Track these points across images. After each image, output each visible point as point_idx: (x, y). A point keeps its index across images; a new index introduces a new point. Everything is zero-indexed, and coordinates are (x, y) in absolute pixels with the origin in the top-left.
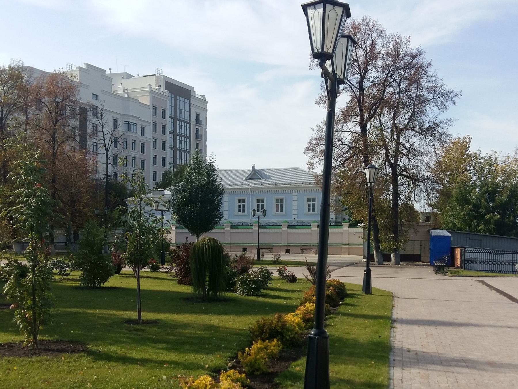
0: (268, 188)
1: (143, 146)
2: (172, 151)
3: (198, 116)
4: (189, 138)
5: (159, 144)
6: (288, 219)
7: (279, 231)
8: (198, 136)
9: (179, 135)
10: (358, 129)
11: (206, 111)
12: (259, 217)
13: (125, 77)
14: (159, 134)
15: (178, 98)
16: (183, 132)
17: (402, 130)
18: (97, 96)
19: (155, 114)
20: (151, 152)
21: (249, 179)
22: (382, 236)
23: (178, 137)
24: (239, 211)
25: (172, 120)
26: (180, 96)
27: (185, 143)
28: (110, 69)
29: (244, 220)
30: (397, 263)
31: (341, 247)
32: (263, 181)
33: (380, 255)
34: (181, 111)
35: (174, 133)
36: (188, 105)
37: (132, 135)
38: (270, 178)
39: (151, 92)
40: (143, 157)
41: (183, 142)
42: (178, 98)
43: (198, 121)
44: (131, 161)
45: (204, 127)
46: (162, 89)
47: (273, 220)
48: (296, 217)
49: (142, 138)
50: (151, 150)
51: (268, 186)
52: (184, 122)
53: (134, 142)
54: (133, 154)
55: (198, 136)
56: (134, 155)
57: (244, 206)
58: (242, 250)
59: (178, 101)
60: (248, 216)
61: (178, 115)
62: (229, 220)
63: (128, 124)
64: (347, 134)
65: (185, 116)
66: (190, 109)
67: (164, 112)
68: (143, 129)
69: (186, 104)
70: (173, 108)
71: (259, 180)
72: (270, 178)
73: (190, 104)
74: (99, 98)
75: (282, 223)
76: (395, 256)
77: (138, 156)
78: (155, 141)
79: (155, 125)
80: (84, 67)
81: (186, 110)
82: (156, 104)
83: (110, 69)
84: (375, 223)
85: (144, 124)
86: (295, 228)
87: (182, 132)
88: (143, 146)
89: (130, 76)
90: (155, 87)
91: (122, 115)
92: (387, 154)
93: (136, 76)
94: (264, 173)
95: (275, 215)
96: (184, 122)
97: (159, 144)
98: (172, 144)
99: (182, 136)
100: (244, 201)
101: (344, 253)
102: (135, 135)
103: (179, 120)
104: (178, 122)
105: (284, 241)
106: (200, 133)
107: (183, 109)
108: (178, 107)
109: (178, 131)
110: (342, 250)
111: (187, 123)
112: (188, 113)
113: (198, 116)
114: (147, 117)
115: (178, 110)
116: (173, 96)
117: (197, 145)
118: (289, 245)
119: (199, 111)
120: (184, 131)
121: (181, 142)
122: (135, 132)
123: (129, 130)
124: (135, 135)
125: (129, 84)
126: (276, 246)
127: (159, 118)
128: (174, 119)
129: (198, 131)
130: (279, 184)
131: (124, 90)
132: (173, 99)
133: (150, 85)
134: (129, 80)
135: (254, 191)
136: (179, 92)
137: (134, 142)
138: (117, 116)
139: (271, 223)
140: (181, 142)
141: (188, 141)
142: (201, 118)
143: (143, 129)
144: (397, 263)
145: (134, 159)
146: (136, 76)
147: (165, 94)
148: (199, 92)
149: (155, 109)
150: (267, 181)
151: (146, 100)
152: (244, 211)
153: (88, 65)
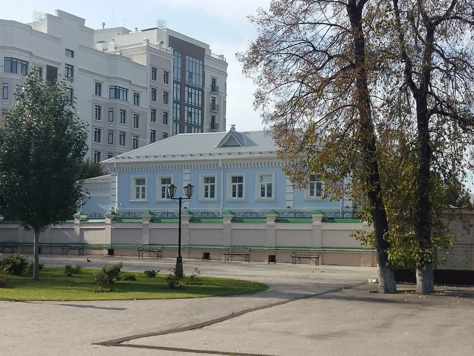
0: (248, 159)
1: (137, 118)
2: (178, 126)
3: (214, 81)
4: (202, 109)
5: (160, 116)
6: (277, 208)
7: (262, 226)
8: (213, 106)
9: (188, 106)
10: (344, 17)
11: (226, 75)
12: (180, 199)
13: (121, 33)
14: (159, 104)
15: (187, 57)
16: (193, 102)
17: (439, 19)
18: (72, 52)
19: (154, 77)
20: (148, 127)
21: (224, 146)
22: (393, 232)
23: (186, 108)
24: (206, 196)
25: (179, 86)
26: (189, 56)
27: (197, 115)
28: (104, 24)
29: (212, 208)
30: (428, 291)
31: (360, 254)
32: (242, 149)
33: (388, 273)
34: (191, 74)
35: (180, 103)
36: (201, 67)
37: (120, 103)
38: (255, 145)
39: (149, 48)
40: (136, 132)
41: (193, 114)
42: (187, 57)
43: (214, 88)
44: (118, 137)
45: (222, 96)
46: (165, 46)
47: (257, 209)
48: (291, 204)
49: (136, 108)
50: (148, 124)
51: (249, 156)
52: (196, 88)
53: (123, 113)
54: (119, 127)
55: (213, 106)
56: (124, 130)
57: (213, 187)
58: (202, 255)
59: (187, 62)
60: (218, 202)
61: (187, 80)
62: (188, 209)
63: (115, 89)
64: (322, 30)
65: (196, 81)
66: (204, 72)
67: (166, 75)
68: (137, 96)
69: (198, 65)
70: (179, 70)
71: (237, 148)
72: (255, 145)
73: (203, 66)
74: (75, 54)
75: (267, 213)
76: (424, 276)
77: (128, 131)
78: (154, 112)
79: (154, 91)
80: (55, 14)
81: (197, 73)
82: (156, 65)
83: (104, 24)
84: (377, 208)
85: (137, 90)
86: (287, 222)
87: (192, 100)
88: (137, 118)
89: (126, 32)
90: (155, 42)
91: (108, 77)
92: (408, 72)
93: (133, 30)
94: (247, 138)
95: (258, 202)
96: (196, 88)
97: (160, 116)
98: (178, 117)
99: (191, 106)
100: (213, 180)
101: (365, 264)
102: (128, 103)
103: (189, 86)
104: (186, 88)
105: (269, 242)
106: (216, 103)
107: (194, 71)
108: (187, 69)
109: (186, 99)
110: (362, 259)
111: (199, 90)
112: (201, 77)
113: (214, 81)
114: (143, 81)
115: (187, 74)
116: (180, 55)
117: (213, 118)
118: (277, 249)
119: (215, 75)
120: (195, 100)
121: (190, 114)
122: (125, 99)
123: (117, 96)
124: (125, 103)
125: (122, 41)
126: (255, 251)
127: (159, 83)
128: (182, 84)
129: (214, 101)
130: (266, 152)
131: (116, 48)
132: (180, 59)
133: (148, 41)
134: (125, 36)
135: (227, 165)
136: (188, 51)
137: (123, 113)
138: (100, 79)
139: (251, 213)
140: (190, 114)
141: (200, 112)
142: (218, 84)
143: (137, 96)
144: (428, 291)
145: (123, 135)
146: (133, 30)
147: (168, 52)
148: (216, 50)
149: (154, 71)
150: (250, 149)
151: (142, 60)
152: (212, 196)
153: (59, 12)
